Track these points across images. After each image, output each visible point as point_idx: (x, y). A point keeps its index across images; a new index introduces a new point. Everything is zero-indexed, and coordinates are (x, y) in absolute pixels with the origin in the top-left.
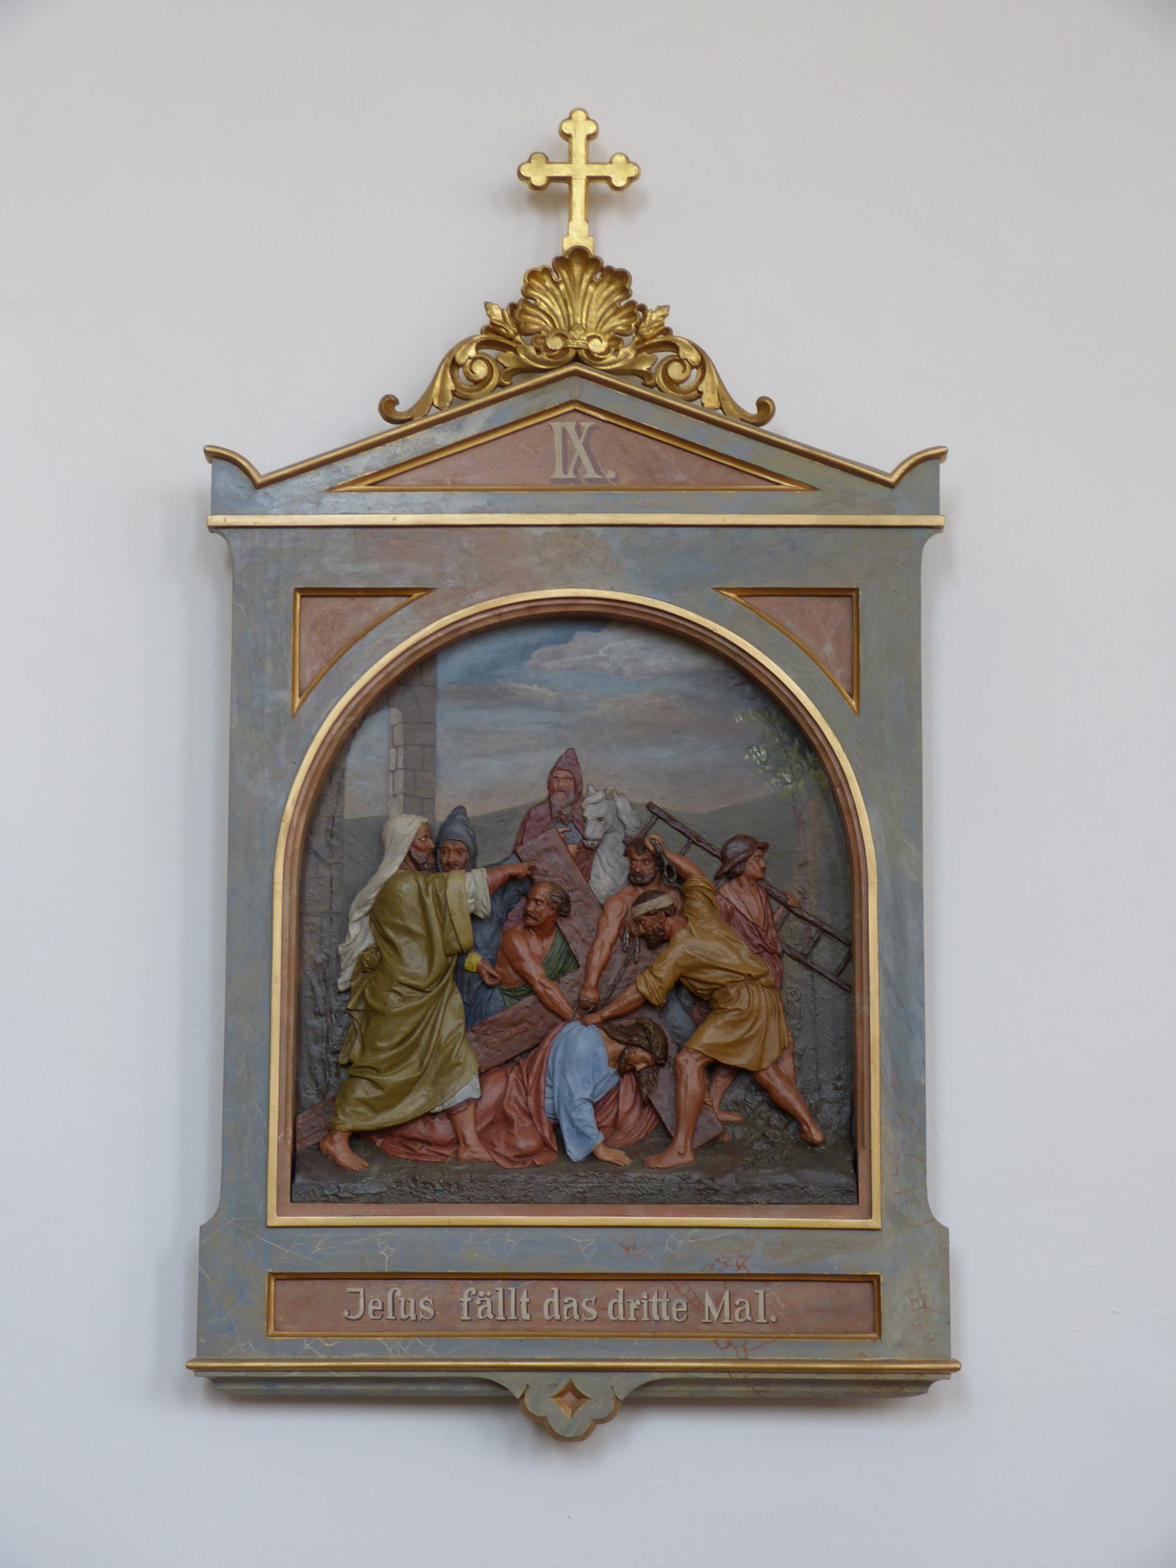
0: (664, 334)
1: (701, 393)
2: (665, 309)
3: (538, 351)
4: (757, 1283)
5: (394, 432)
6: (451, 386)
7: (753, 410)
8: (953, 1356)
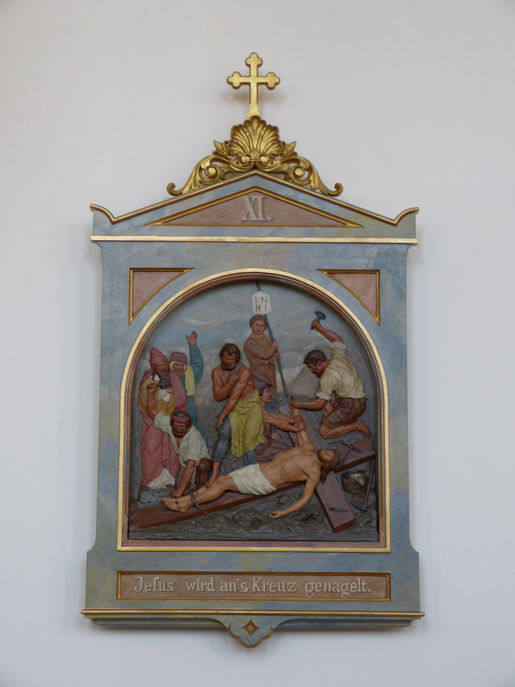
1: (310, 181)
3: (238, 163)
5: (173, 200)
6: (198, 178)
7: (334, 190)
8: (421, 610)
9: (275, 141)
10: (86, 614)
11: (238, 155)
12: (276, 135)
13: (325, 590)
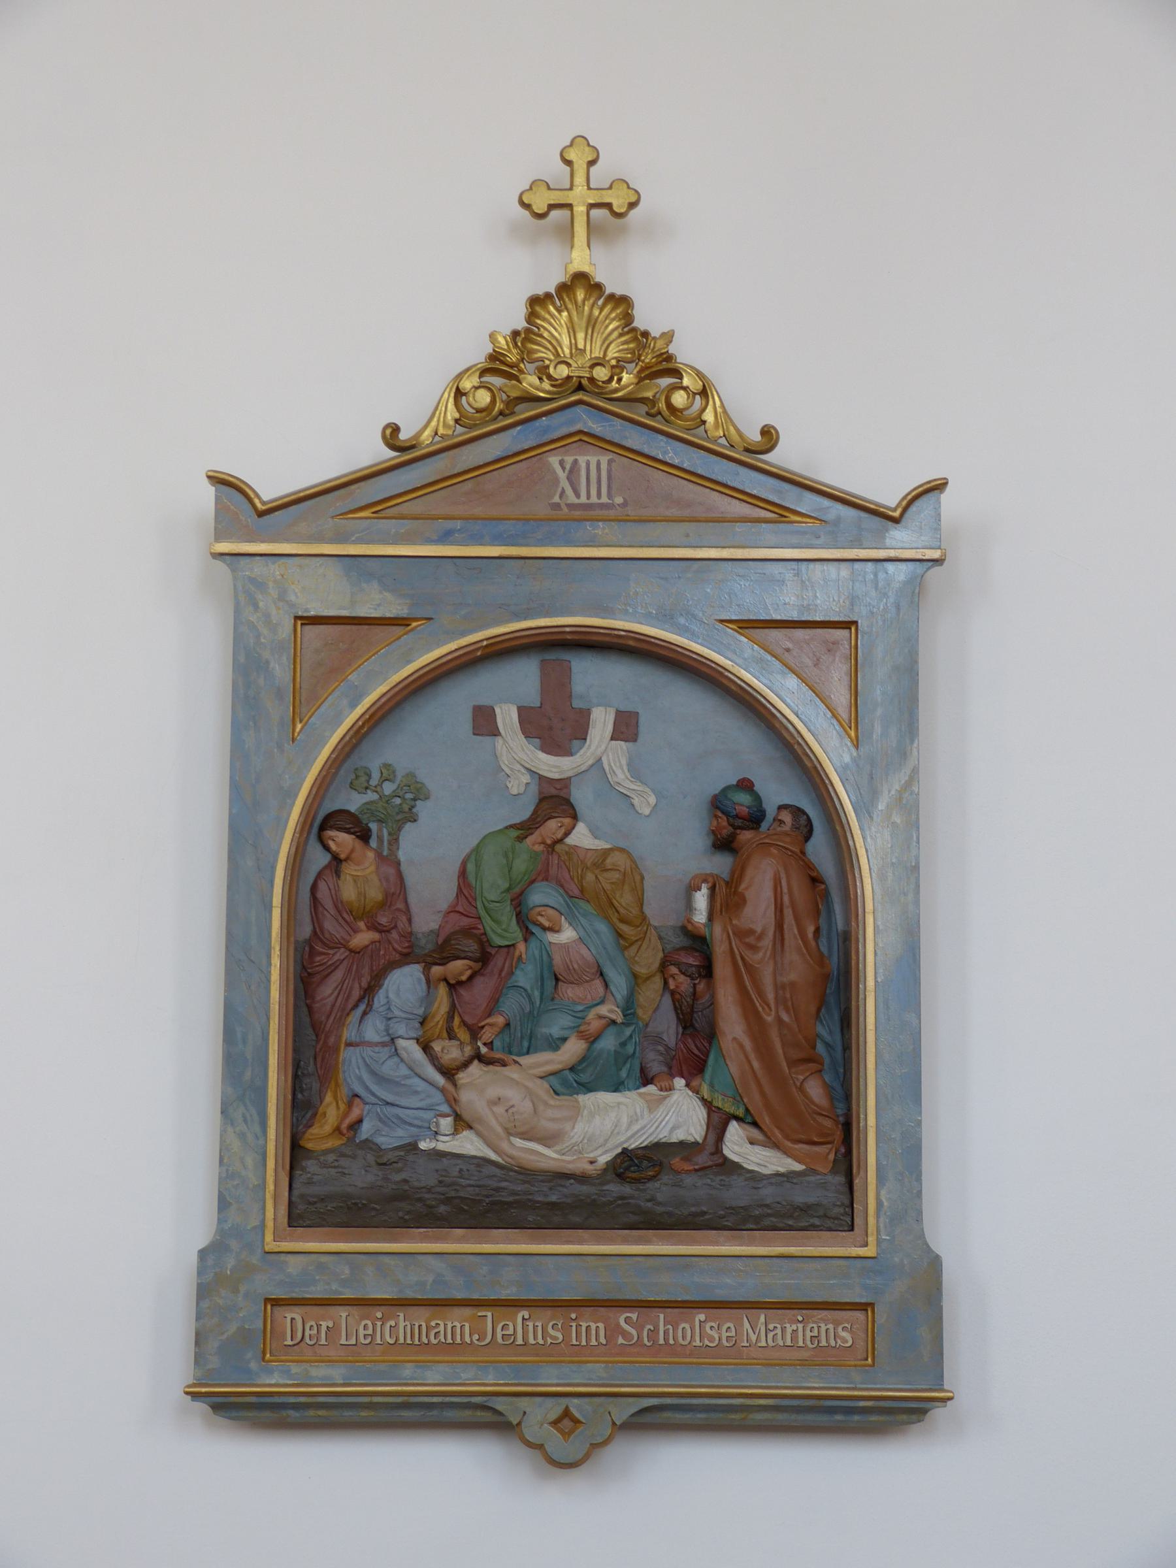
0: (667, 362)
1: (704, 422)
2: (669, 336)
4: (539, 1308)
7: (755, 436)
8: (946, 1387)
9: (626, 329)
10: (195, 1396)
11: (543, 361)
12: (628, 318)
13: (458, 1341)
